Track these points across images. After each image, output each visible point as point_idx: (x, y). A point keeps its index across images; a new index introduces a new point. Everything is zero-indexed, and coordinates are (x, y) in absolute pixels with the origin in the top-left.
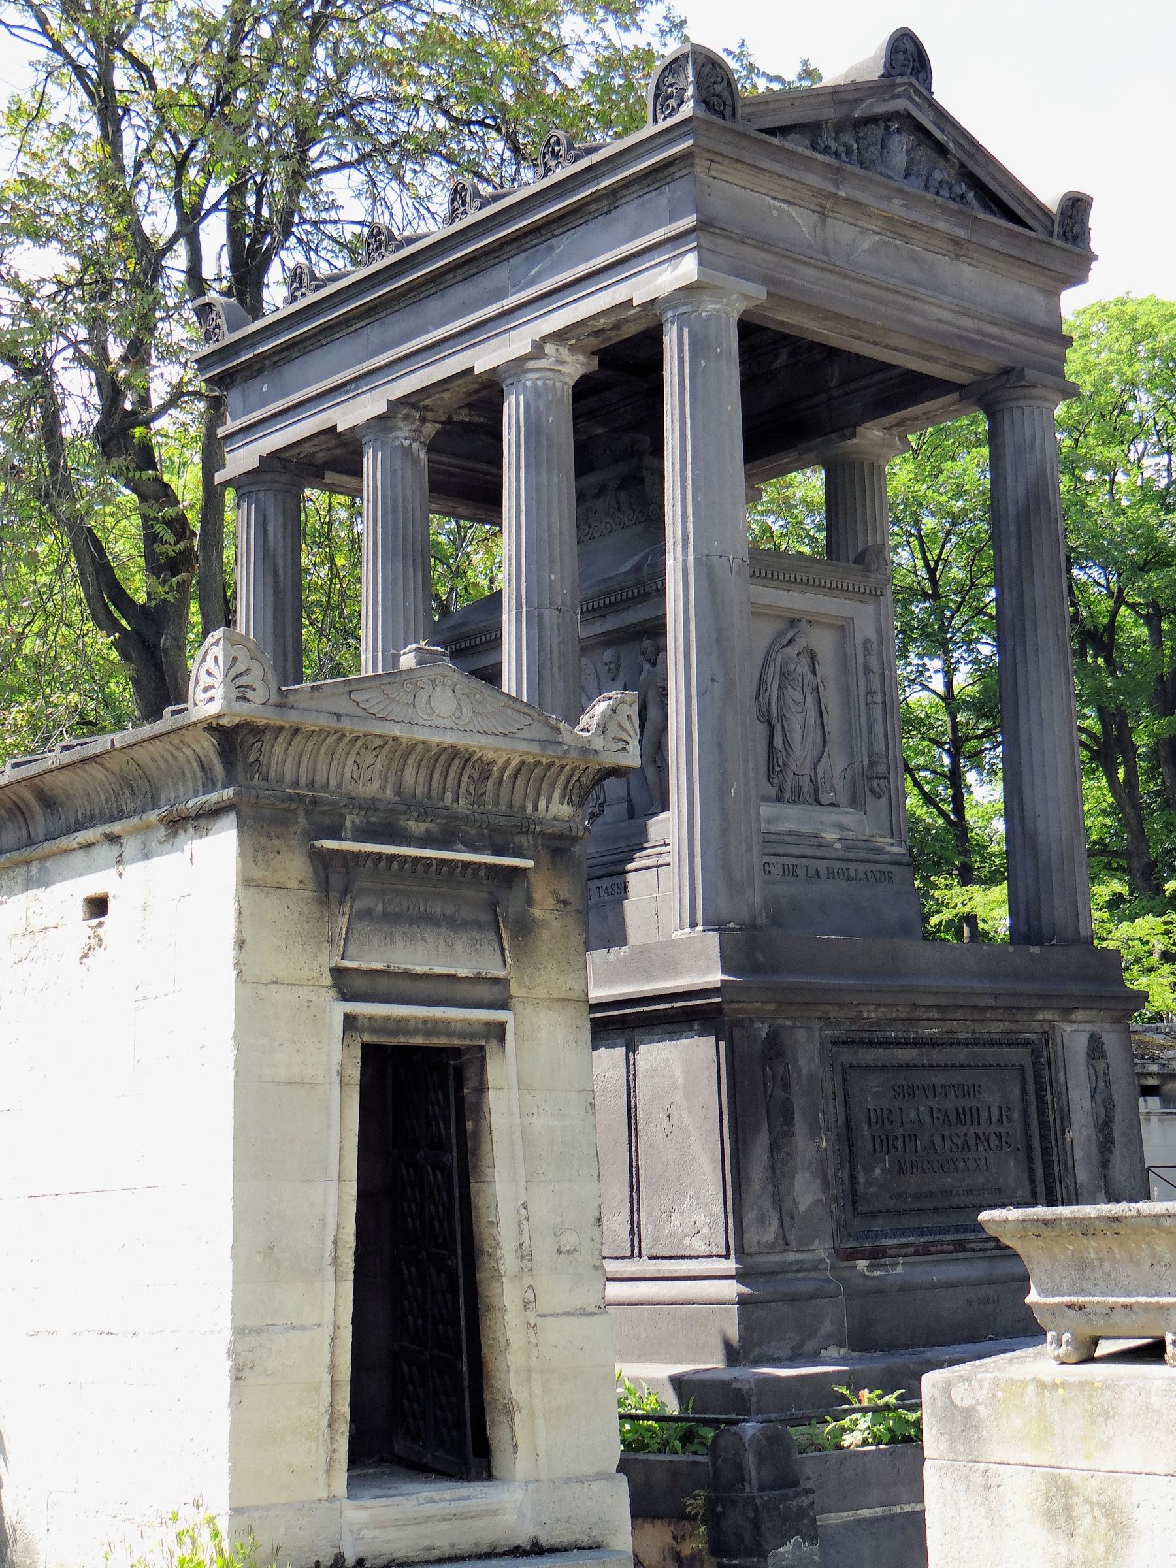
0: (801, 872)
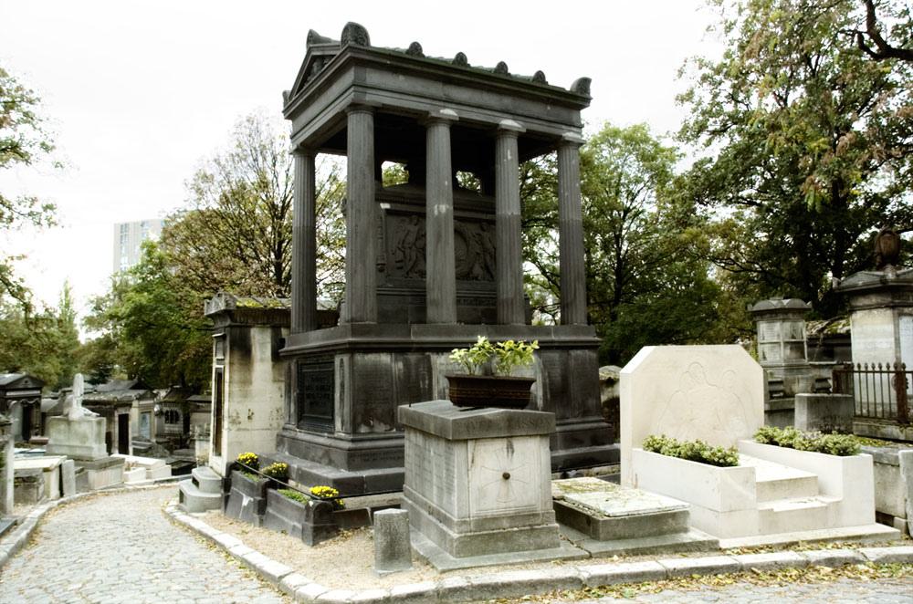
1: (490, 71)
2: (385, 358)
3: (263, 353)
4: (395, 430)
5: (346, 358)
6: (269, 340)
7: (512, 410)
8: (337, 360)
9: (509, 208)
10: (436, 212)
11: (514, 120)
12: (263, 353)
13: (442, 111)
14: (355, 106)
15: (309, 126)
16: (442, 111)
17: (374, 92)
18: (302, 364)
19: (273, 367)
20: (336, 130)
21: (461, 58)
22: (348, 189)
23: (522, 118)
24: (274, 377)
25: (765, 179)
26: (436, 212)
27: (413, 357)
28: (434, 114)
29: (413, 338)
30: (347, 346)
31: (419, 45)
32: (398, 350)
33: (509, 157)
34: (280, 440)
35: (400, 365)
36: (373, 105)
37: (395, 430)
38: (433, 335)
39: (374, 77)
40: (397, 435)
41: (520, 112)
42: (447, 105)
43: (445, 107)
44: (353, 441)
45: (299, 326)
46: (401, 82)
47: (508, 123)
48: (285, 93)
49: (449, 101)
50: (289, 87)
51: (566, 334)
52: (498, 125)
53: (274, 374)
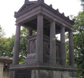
1: (47, 6)
2: (45, 71)
5: (37, 71)
6: (3, 66)
7: (20, 67)
8: (33, 71)
10: (53, 40)
14: (41, 14)
17: (44, 12)
19: (3, 72)
20: (35, 18)
21: (51, 5)
22: (26, 27)
26: (53, 40)
27: (50, 71)
29: (50, 67)
32: (48, 69)
35: (48, 73)
39: (44, 9)
43: (55, 18)
46: (48, 11)
47: (64, 24)
48: (15, 12)
49: (65, 23)
50: (17, 11)
52: (70, 29)
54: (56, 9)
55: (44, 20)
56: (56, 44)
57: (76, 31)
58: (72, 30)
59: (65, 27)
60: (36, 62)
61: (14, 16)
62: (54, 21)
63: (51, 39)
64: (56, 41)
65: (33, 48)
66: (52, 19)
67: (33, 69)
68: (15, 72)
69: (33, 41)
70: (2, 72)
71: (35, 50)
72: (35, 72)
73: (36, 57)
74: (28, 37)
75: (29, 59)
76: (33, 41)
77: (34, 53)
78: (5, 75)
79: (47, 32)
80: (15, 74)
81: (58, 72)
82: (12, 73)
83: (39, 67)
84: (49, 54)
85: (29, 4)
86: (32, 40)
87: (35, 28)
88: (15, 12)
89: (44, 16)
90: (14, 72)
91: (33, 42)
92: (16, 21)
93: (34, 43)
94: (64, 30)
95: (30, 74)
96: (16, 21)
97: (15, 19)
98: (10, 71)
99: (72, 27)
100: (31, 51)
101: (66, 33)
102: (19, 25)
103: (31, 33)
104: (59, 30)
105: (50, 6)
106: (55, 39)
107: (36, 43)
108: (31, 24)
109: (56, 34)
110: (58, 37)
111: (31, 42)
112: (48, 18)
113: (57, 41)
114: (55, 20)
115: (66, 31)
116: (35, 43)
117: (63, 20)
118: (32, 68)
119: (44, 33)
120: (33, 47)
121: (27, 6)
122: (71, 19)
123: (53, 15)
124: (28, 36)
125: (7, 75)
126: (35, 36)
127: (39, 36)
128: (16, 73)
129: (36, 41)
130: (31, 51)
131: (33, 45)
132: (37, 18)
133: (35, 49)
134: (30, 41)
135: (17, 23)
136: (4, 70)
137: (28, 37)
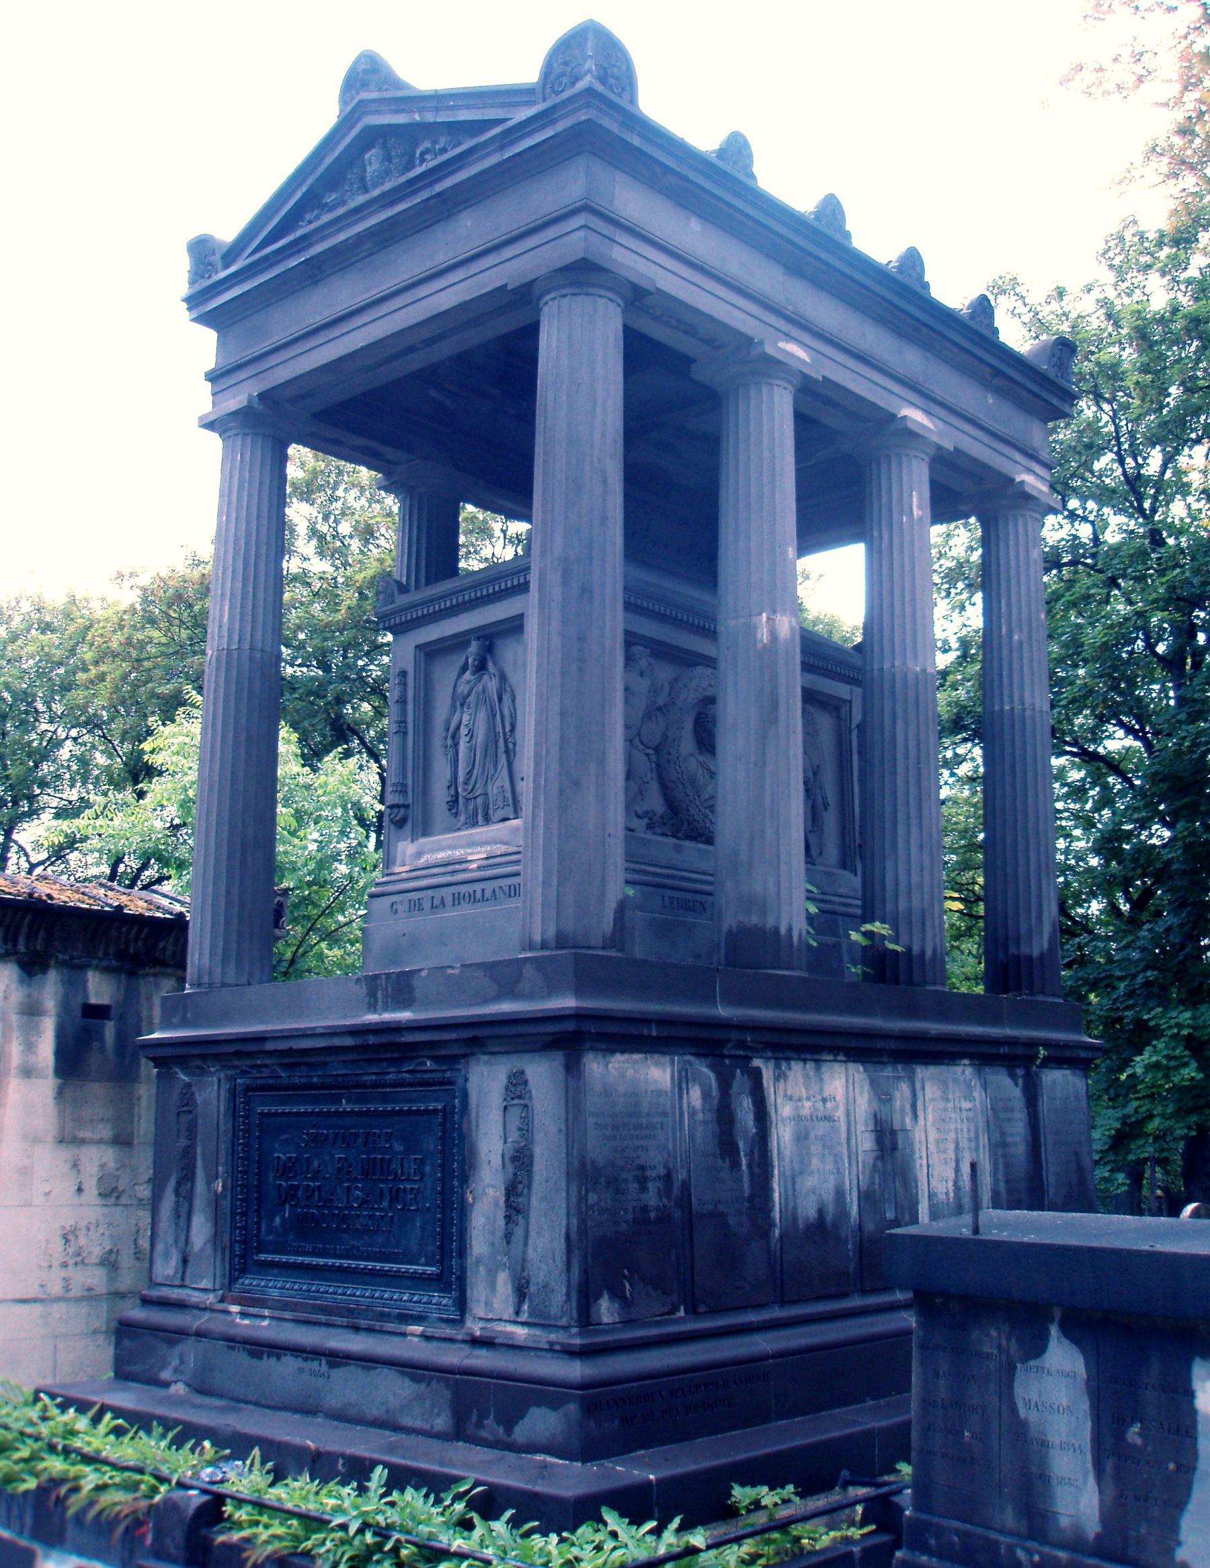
0: (427, 905)
3: (30, 1047)
4: (682, 1313)
5: (541, 1073)
8: (486, 1081)
9: (915, 657)
11: (926, 412)
12: (30, 1047)
13: (781, 345)
15: (335, 332)
16: (781, 345)
18: (248, 1089)
19: (60, 1094)
23: (942, 413)
24: (62, 1129)
25: (187, 795)
26: (764, 635)
28: (769, 350)
30: (348, 1041)
31: (746, 145)
33: (916, 512)
34: (138, 1341)
36: (634, 279)
37: (682, 1313)
38: (767, 1005)
40: (689, 1326)
41: (939, 393)
42: (795, 332)
43: (789, 337)
44: (584, 1353)
45: (225, 961)
47: (915, 415)
48: (201, 249)
50: (227, 231)
51: (888, 1013)
52: (893, 417)
53: (61, 1114)
54: (801, 199)
55: (640, 353)
56: (810, 697)
57: (1073, 503)
58: (1025, 498)
59: (939, 448)
60: (531, 946)
61: (193, 301)
62: (773, 366)
63: (728, 624)
64: (802, 637)
65: (472, 749)
66: (748, 341)
67: (481, 1037)
68: (233, 1093)
69: (474, 647)
70: (46, 1086)
71: (503, 779)
72: (517, 1087)
73: (534, 874)
74: (402, 600)
75: (416, 906)
76: (474, 647)
77: (487, 820)
78: (81, 1134)
79: (674, 508)
80: (233, 1111)
81: (104, 1454)
82: (187, 1099)
83: (578, 1015)
84: (703, 835)
85: (412, 133)
86: (458, 643)
87: (509, 483)
88: (201, 249)
89: (636, 297)
90: (212, 1093)
91: (481, 667)
92: (213, 377)
93: (492, 685)
94: (918, 502)
95: (447, 1113)
96: (213, 377)
97: (204, 346)
98: (148, 1070)
99: (1032, 456)
100: (440, 794)
101: (958, 541)
102: (270, 420)
103: (433, 544)
104: (836, 500)
105: (722, 153)
106: (785, 625)
107: (513, 678)
108: (445, 416)
109: (802, 551)
110: (833, 588)
111: (448, 678)
112: (691, 331)
113: (818, 654)
114: (796, 351)
115: (946, 506)
116: (503, 678)
117: (912, 360)
118: (466, 1034)
119: (640, 543)
120: (471, 734)
121: (373, 159)
122: (1014, 334)
123: (767, 278)
124: (403, 589)
125: (106, 1132)
126: (506, 581)
127: (565, 582)
128: (240, 1101)
129: (529, 664)
130: (440, 794)
131: (482, 715)
132: (532, 331)
133: (503, 760)
134: (431, 653)
135: (236, 401)
136: (71, 1061)
137: (402, 600)
